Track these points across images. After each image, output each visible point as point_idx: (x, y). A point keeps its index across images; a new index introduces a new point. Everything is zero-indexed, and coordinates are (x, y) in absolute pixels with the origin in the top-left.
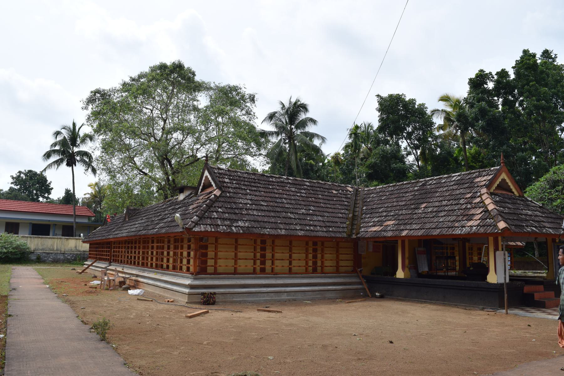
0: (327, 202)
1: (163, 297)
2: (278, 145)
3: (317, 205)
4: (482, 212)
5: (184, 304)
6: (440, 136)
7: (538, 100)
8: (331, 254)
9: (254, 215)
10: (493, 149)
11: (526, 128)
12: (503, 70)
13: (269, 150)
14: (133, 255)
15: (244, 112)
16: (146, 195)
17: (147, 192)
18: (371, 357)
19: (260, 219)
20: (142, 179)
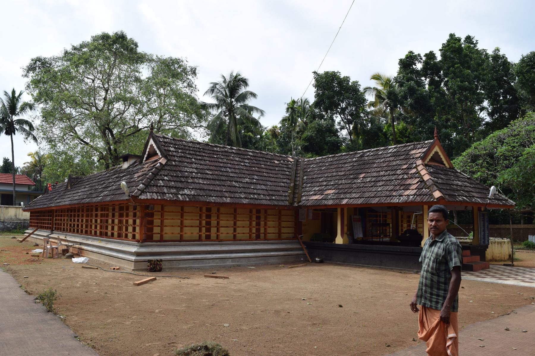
0: (269, 171)
1: (109, 264)
2: (218, 117)
3: (260, 174)
4: (418, 182)
5: (130, 271)
6: (371, 113)
7: (462, 82)
8: (273, 221)
9: (200, 183)
10: (420, 125)
11: (450, 107)
12: (431, 53)
13: (209, 122)
14: (76, 223)
15: (185, 84)
16: (87, 165)
17: (88, 161)
18: (325, 322)
19: (205, 187)
20: (82, 148)
